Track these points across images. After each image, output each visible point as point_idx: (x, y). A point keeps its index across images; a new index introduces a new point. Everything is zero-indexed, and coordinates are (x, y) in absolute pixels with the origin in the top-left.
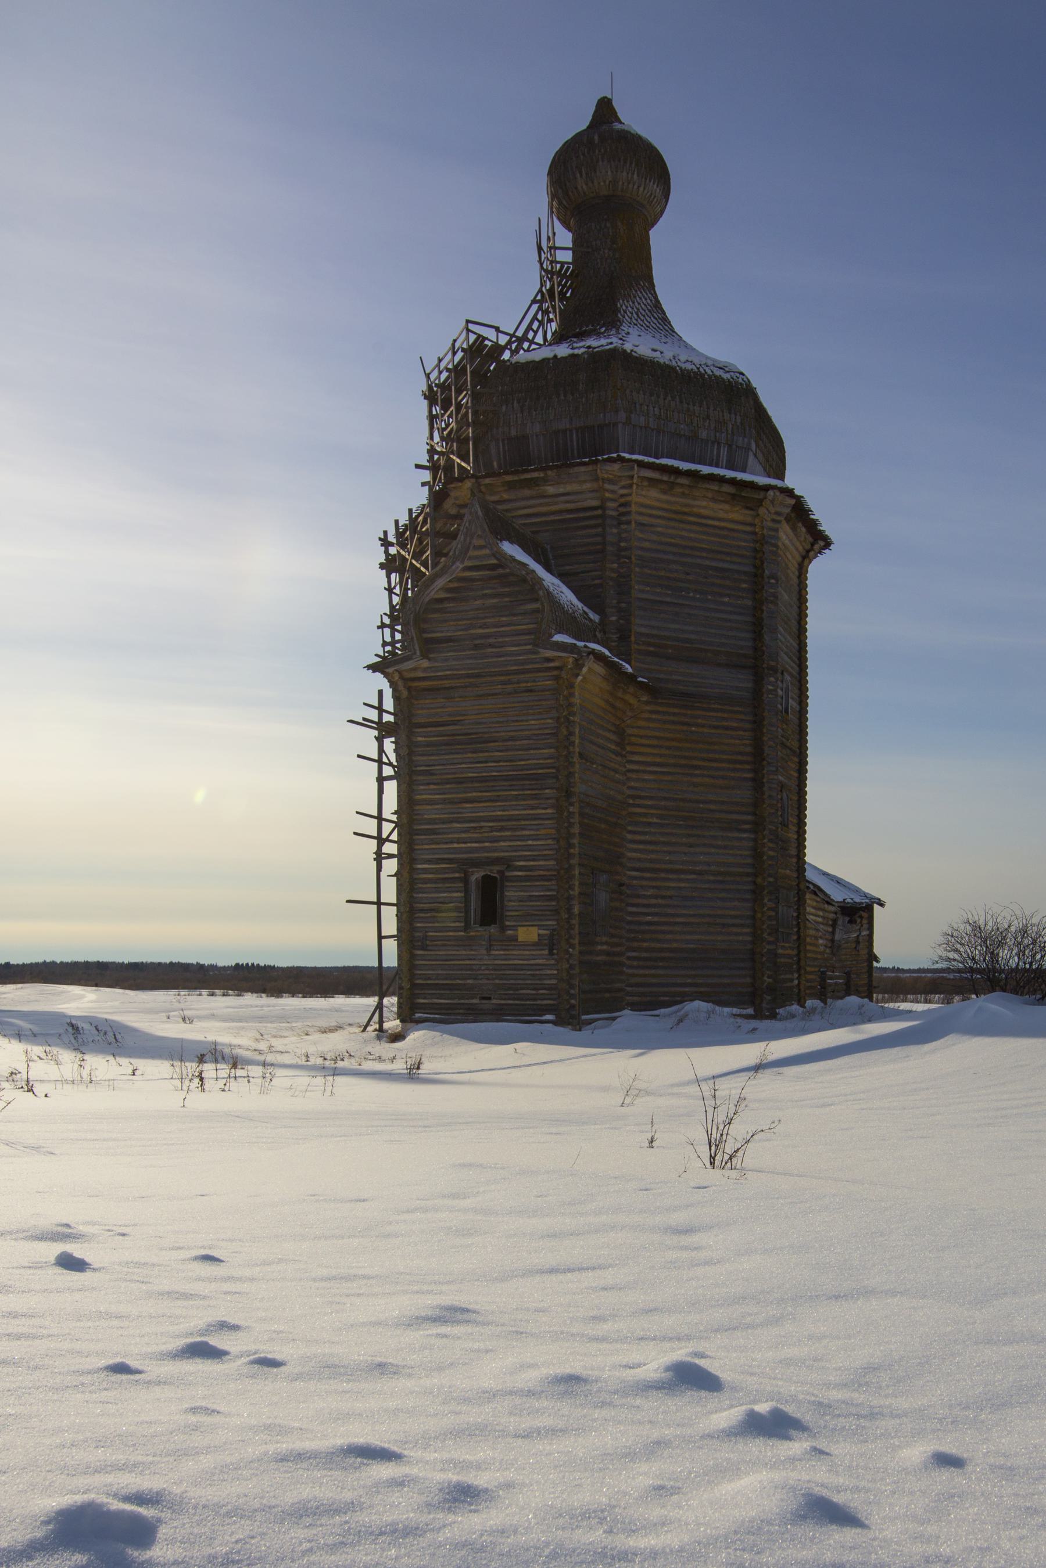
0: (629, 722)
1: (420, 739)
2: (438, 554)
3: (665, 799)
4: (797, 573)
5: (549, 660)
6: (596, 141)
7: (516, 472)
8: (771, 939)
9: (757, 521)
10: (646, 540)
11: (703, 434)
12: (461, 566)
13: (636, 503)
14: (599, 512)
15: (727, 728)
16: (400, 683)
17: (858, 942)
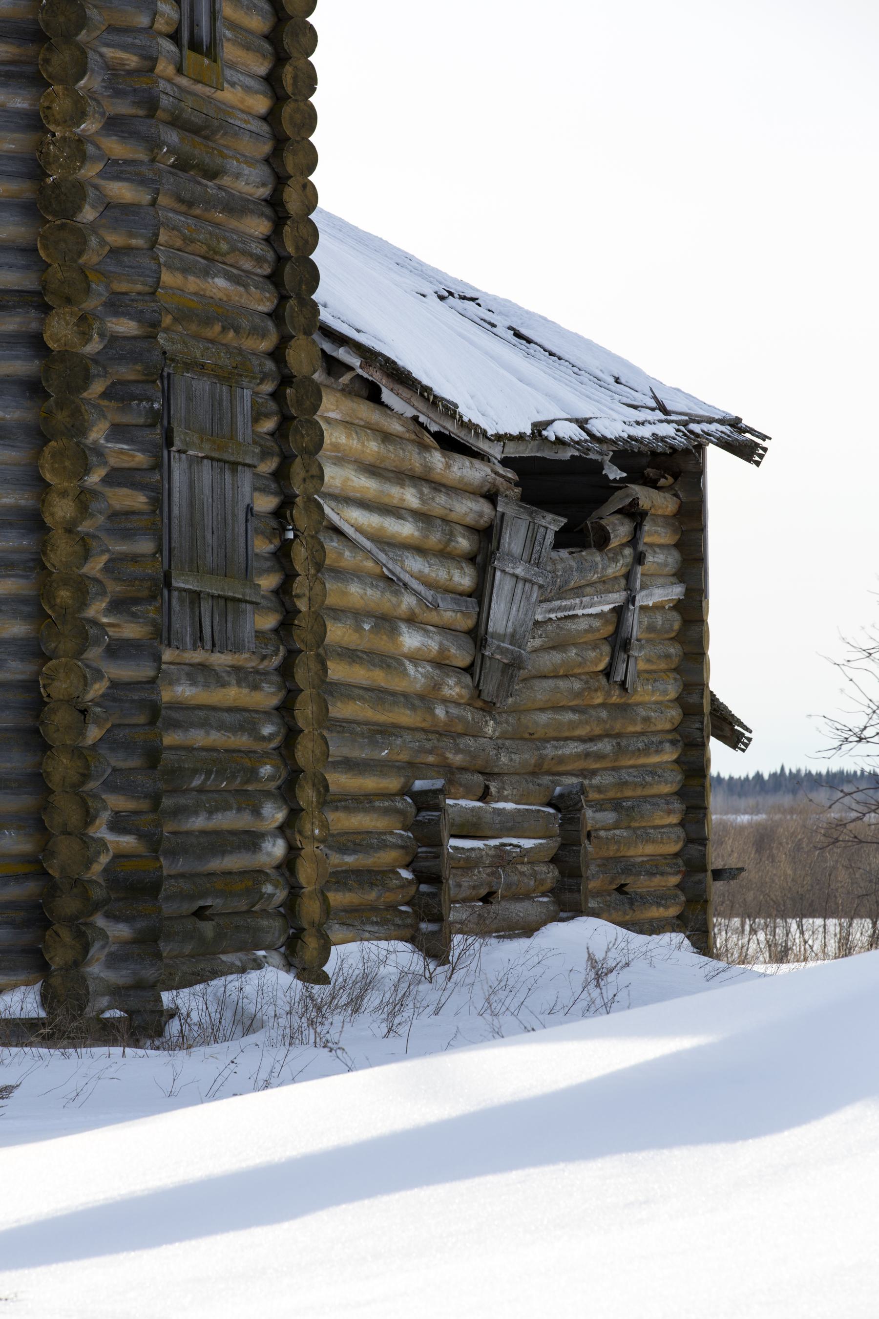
8: (132, 631)
17: (619, 643)
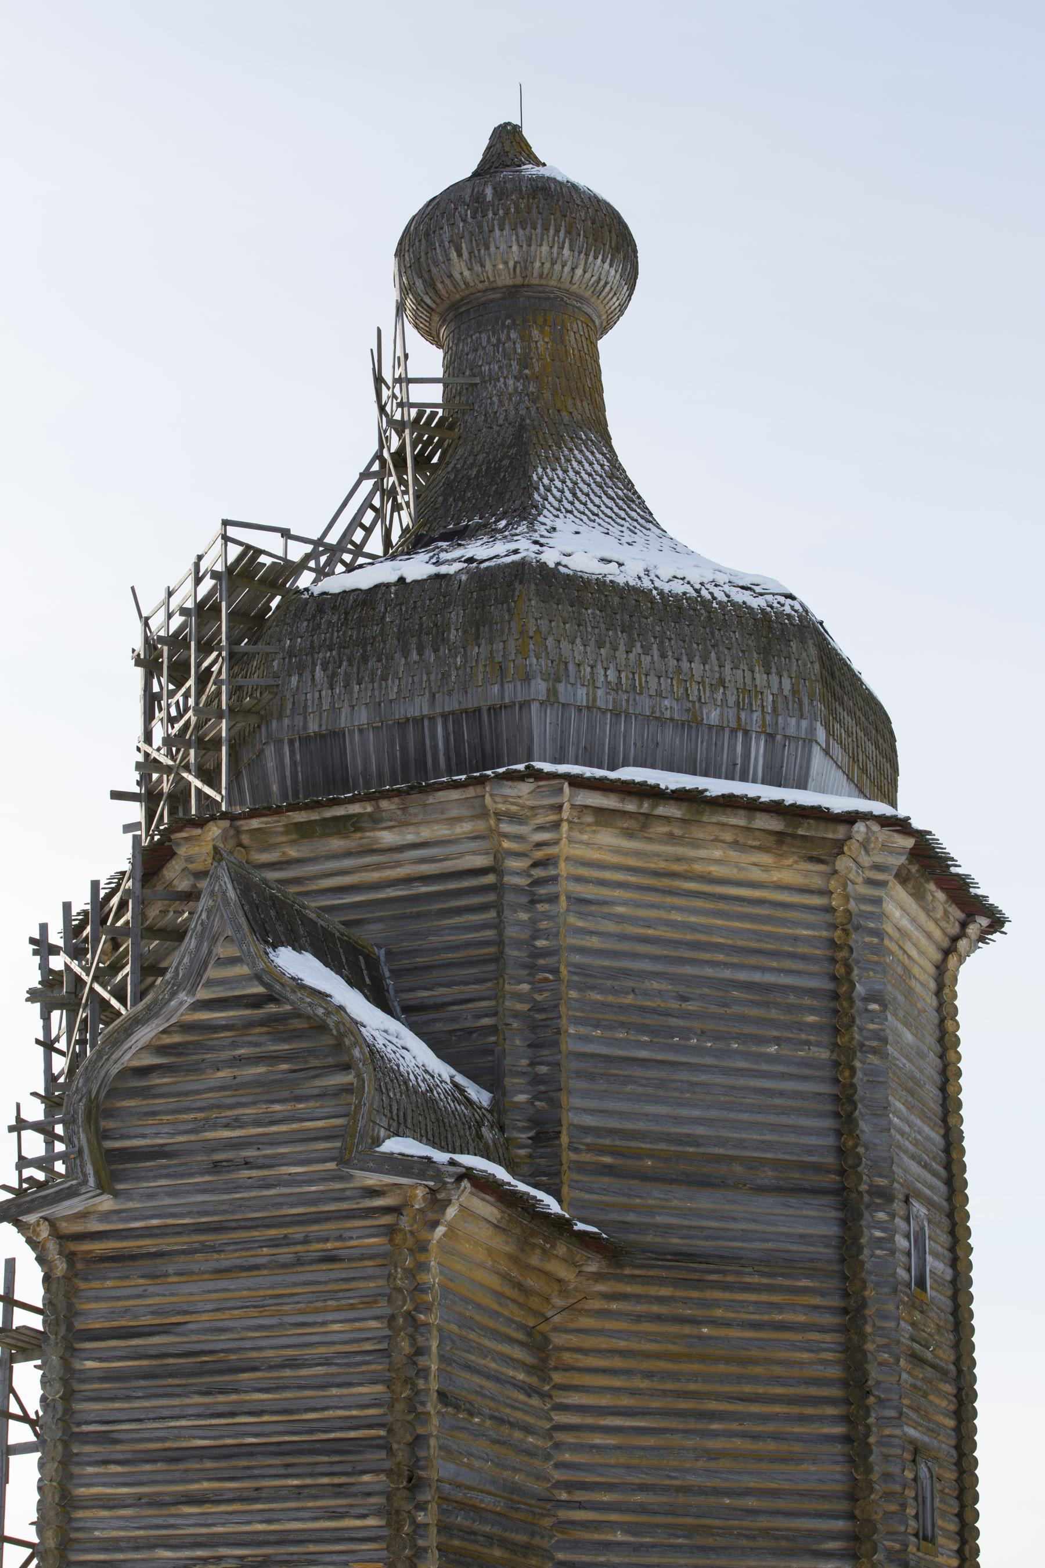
0: (557, 1319)
1: (90, 1364)
2: (150, 969)
3: (642, 1488)
4: (932, 985)
5: (373, 1192)
6: (489, 198)
7: (316, 805)
9: (833, 884)
10: (592, 933)
11: (713, 716)
12: (190, 1000)
13: (568, 859)
14: (490, 879)
15: (781, 1327)
16: (52, 1246)
